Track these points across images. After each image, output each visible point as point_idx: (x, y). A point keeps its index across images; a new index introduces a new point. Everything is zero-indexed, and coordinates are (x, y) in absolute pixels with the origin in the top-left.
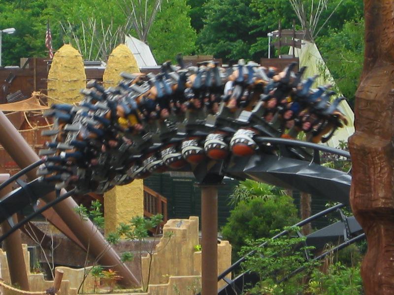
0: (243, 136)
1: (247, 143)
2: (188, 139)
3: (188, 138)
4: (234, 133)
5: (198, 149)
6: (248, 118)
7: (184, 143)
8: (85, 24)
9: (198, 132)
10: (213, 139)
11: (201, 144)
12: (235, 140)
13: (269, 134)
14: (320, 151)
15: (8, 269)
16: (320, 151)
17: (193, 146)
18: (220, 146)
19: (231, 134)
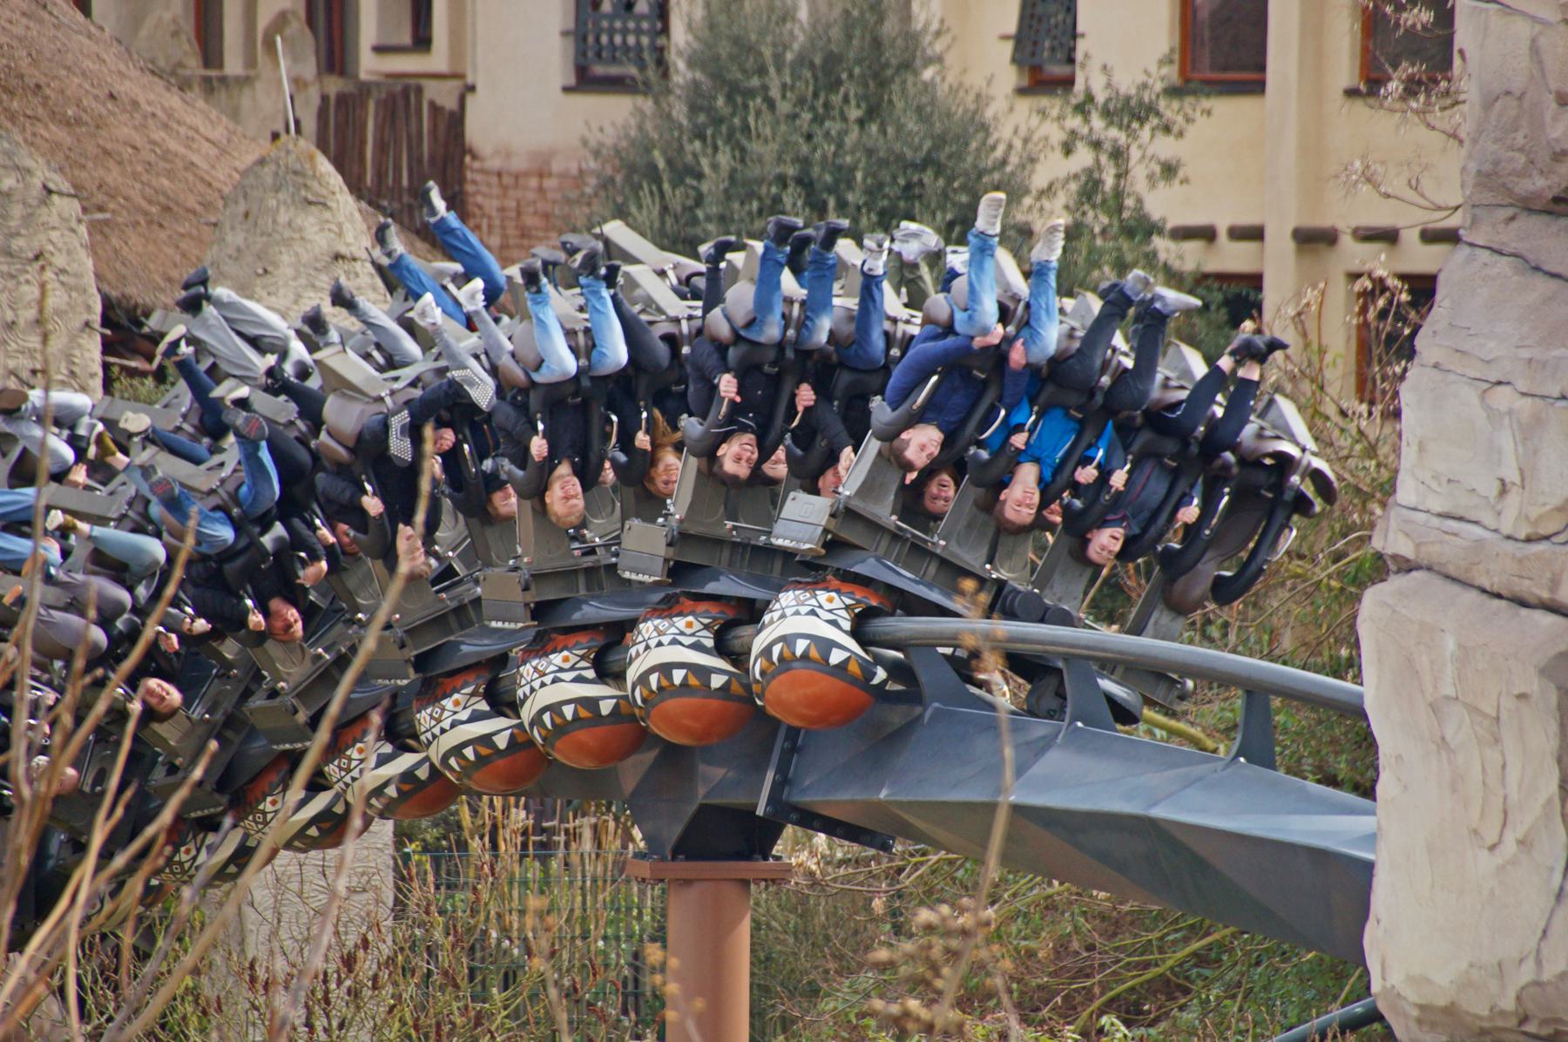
0: (808, 619)
1: (827, 661)
2: (668, 608)
3: (541, 645)
4: (765, 606)
5: (499, 728)
6: (659, 565)
7: (647, 629)
8: (420, 161)
9: (593, 611)
10: (668, 645)
11: (607, 669)
12: (767, 652)
13: (935, 596)
14: (1276, 702)
15: (847, 843)
16: (1276, 702)
17: (579, 680)
18: (493, 746)
19: (752, 612)
